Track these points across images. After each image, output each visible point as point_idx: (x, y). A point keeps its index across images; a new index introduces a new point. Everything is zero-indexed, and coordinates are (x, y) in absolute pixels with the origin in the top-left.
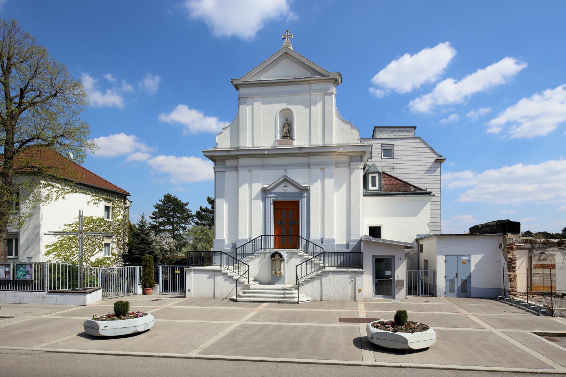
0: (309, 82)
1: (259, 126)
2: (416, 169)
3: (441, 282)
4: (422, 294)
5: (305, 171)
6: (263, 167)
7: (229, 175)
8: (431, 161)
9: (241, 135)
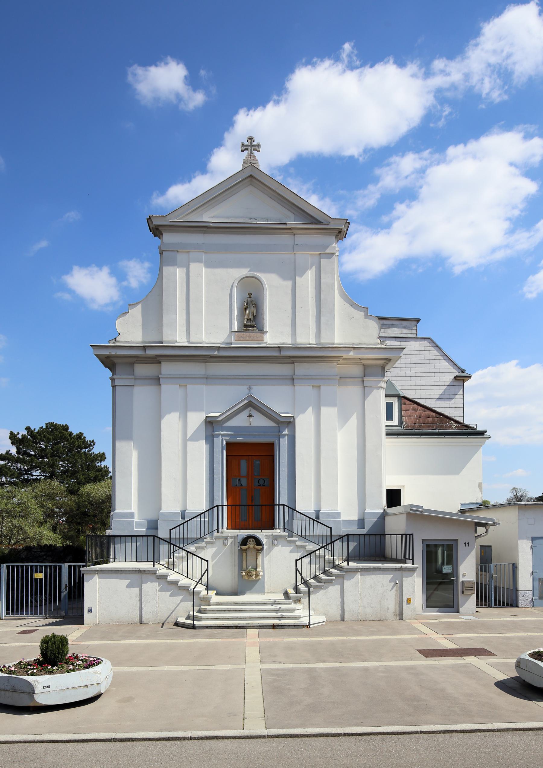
0: (292, 231)
1: (200, 306)
2: (424, 392)
3: (525, 583)
4: (495, 604)
5: (285, 389)
6: (208, 379)
7: (142, 394)
8: (448, 379)
9: (165, 319)
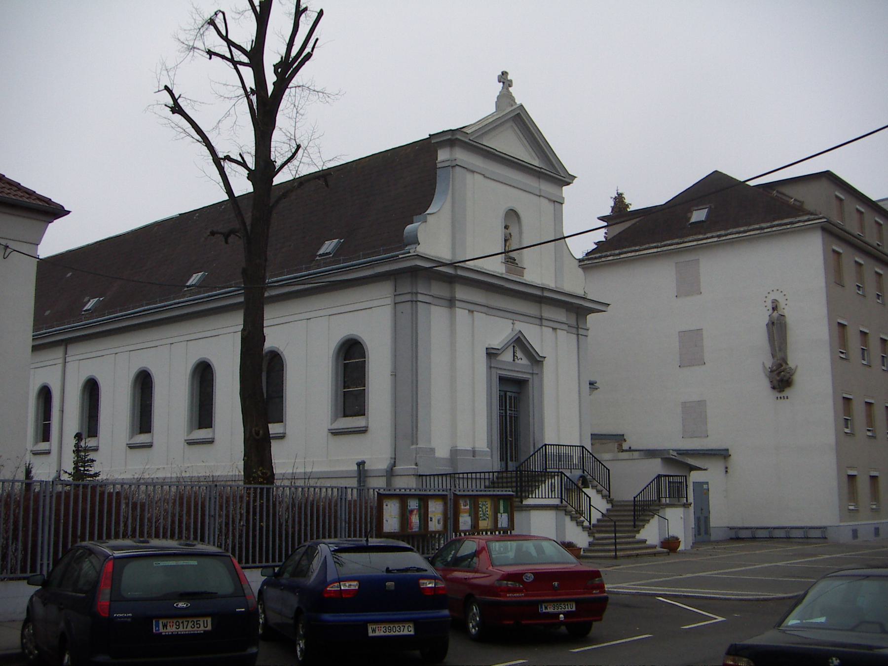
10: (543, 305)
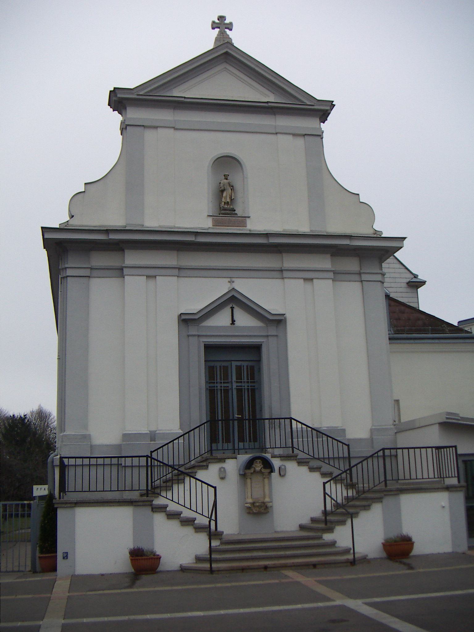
6: (180, 271)
10: (284, 255)
